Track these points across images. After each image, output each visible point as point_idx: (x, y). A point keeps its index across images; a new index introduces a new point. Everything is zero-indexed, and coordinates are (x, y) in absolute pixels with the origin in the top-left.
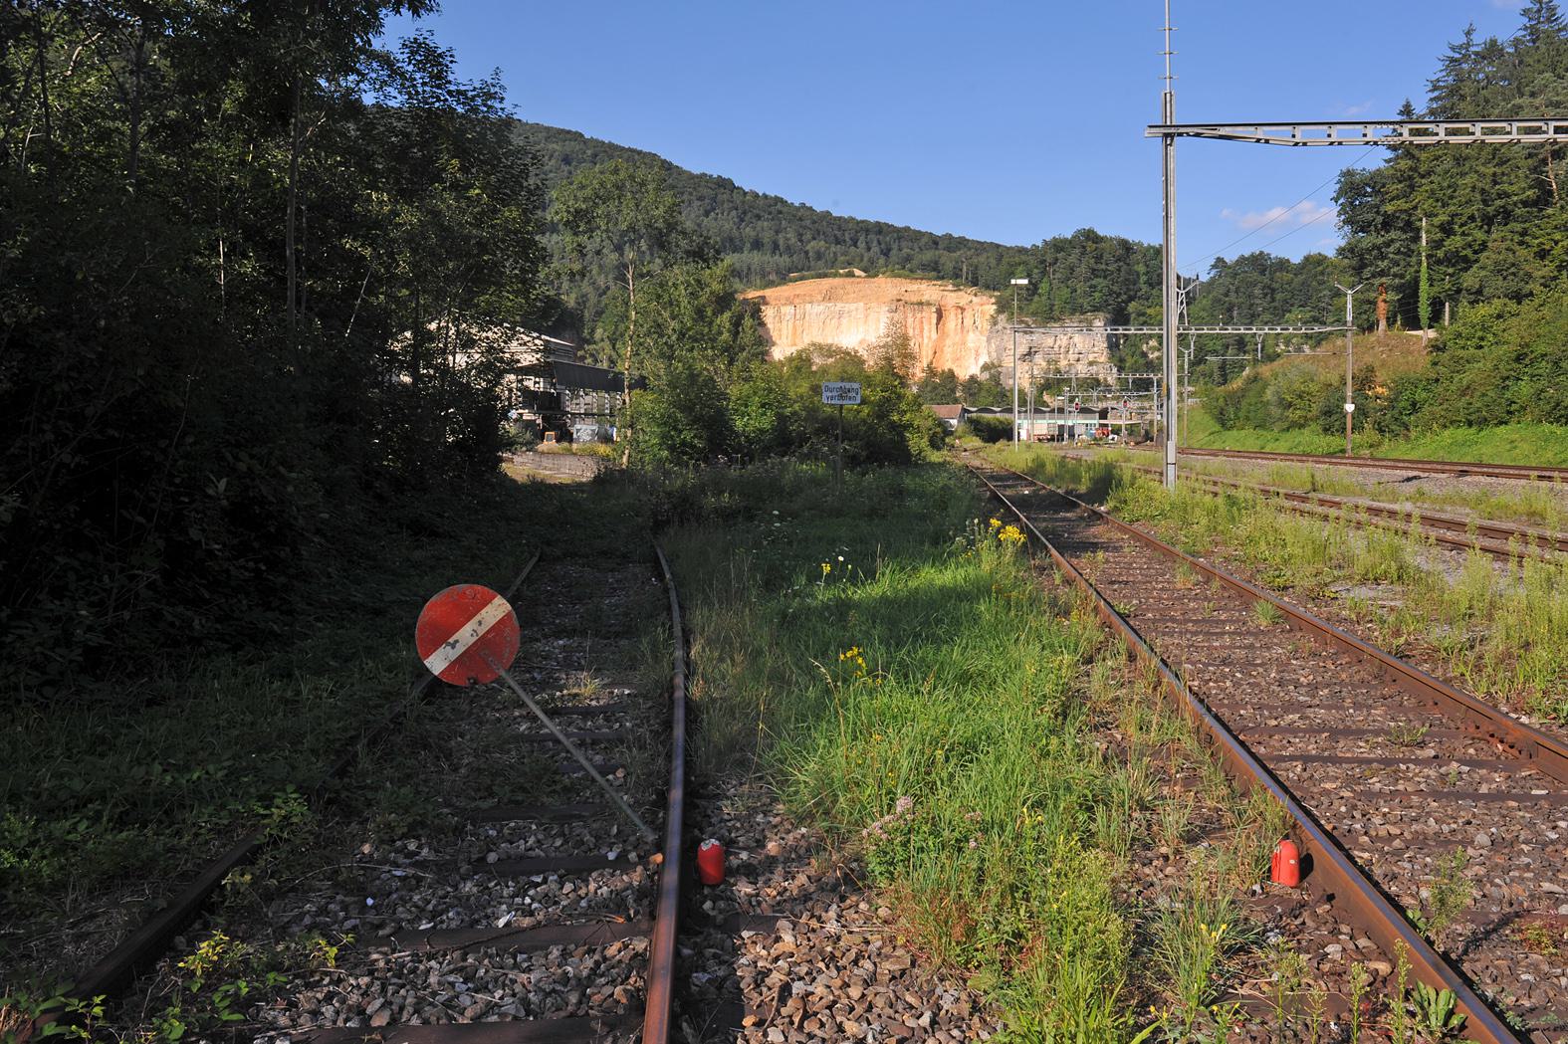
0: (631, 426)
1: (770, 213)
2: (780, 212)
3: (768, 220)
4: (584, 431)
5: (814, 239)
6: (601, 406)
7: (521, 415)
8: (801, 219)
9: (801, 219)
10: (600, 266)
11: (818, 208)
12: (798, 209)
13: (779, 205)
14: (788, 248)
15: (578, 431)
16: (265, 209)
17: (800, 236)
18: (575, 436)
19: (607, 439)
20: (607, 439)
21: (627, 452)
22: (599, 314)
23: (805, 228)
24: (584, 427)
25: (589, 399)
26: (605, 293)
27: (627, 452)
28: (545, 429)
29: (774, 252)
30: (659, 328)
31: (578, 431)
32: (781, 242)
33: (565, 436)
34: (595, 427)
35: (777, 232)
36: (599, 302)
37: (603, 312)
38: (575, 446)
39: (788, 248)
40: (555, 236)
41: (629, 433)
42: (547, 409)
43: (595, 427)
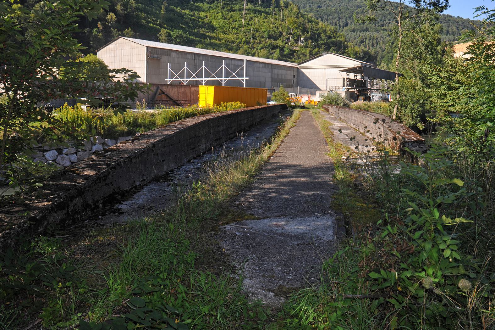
0: (399, 94)
1: (445, 21)
2: (450, 20)
3: (445, 23)
4: (376, 96)
5: (463, 29)
6: (383, 87)
7: (348, 89)
8: (458, 22)
9: (458, 22)
10: (383, 41)
11: (464, 18)
12: (456, 18)
13: (449, 18)
14: (453, 32)
15: (373, 96)
16: (474, 164)
17: (457, 28)
18: (371, 98)
19: (386, 100)
20: (386, 100)
21: (396, 106)
22: (383, 58)
23: (459, 25)
24: (376, 94)
25: (380, 84)
26: (385, 50)
27: (396, 106)
28: (359, 96)
29: (447, 34)
30: (414, 44)
31: (373, 96)
32: (450, 31)
33: (367, 98)
34: (381, 95)
35: (448, 27)
36: (383, 54)
37: (384, 57)
38: (371, 103)
39: (453, 32)
40: (367, 32)
41: (398, 97)
42: (360, 87)
43: (381, 95)
